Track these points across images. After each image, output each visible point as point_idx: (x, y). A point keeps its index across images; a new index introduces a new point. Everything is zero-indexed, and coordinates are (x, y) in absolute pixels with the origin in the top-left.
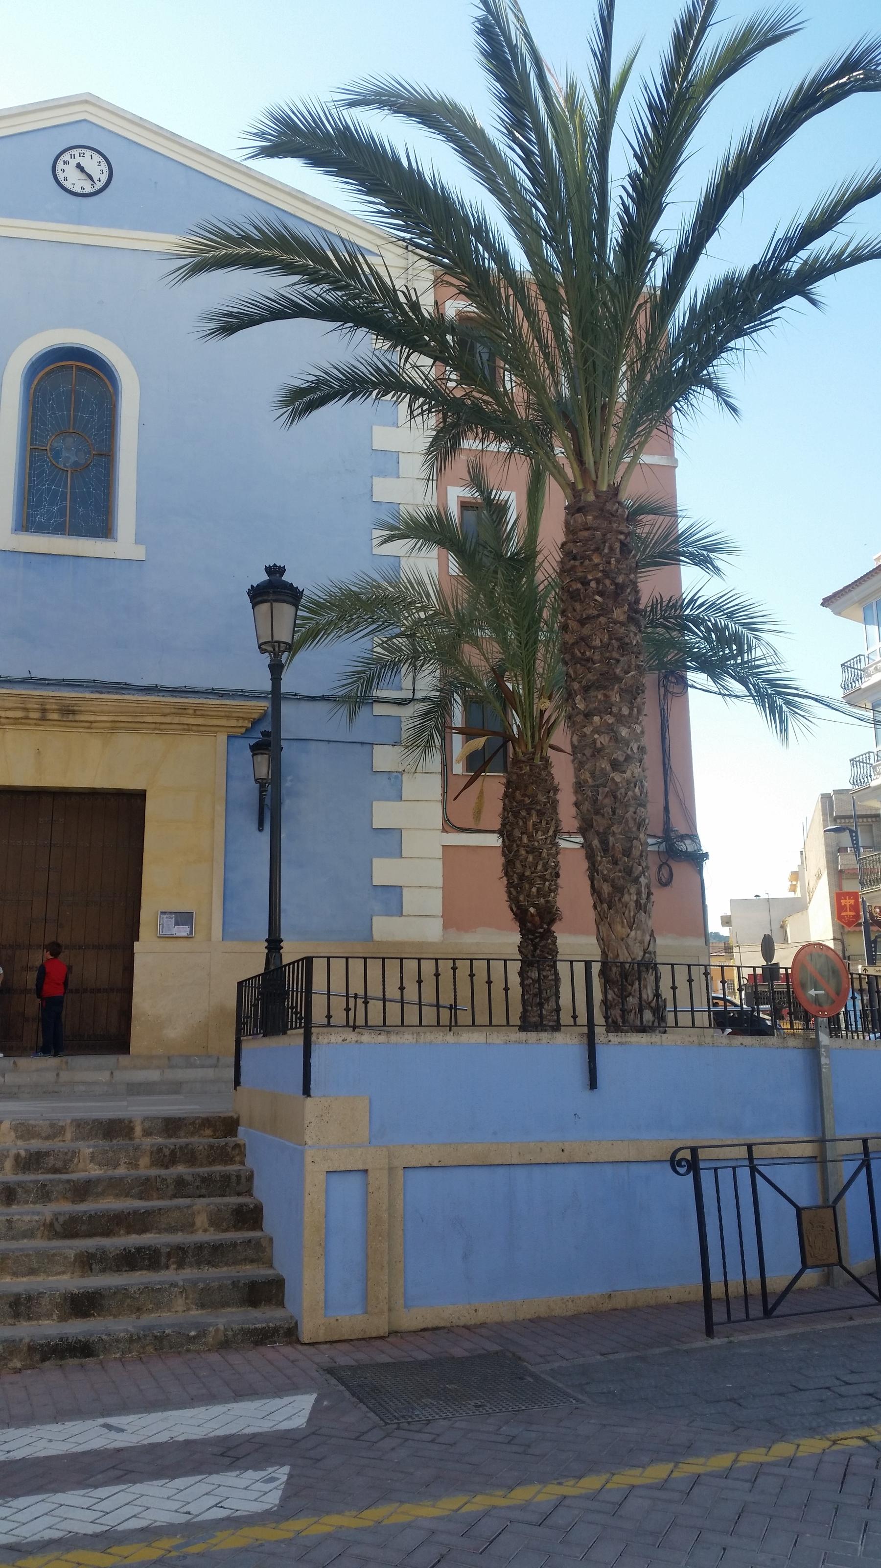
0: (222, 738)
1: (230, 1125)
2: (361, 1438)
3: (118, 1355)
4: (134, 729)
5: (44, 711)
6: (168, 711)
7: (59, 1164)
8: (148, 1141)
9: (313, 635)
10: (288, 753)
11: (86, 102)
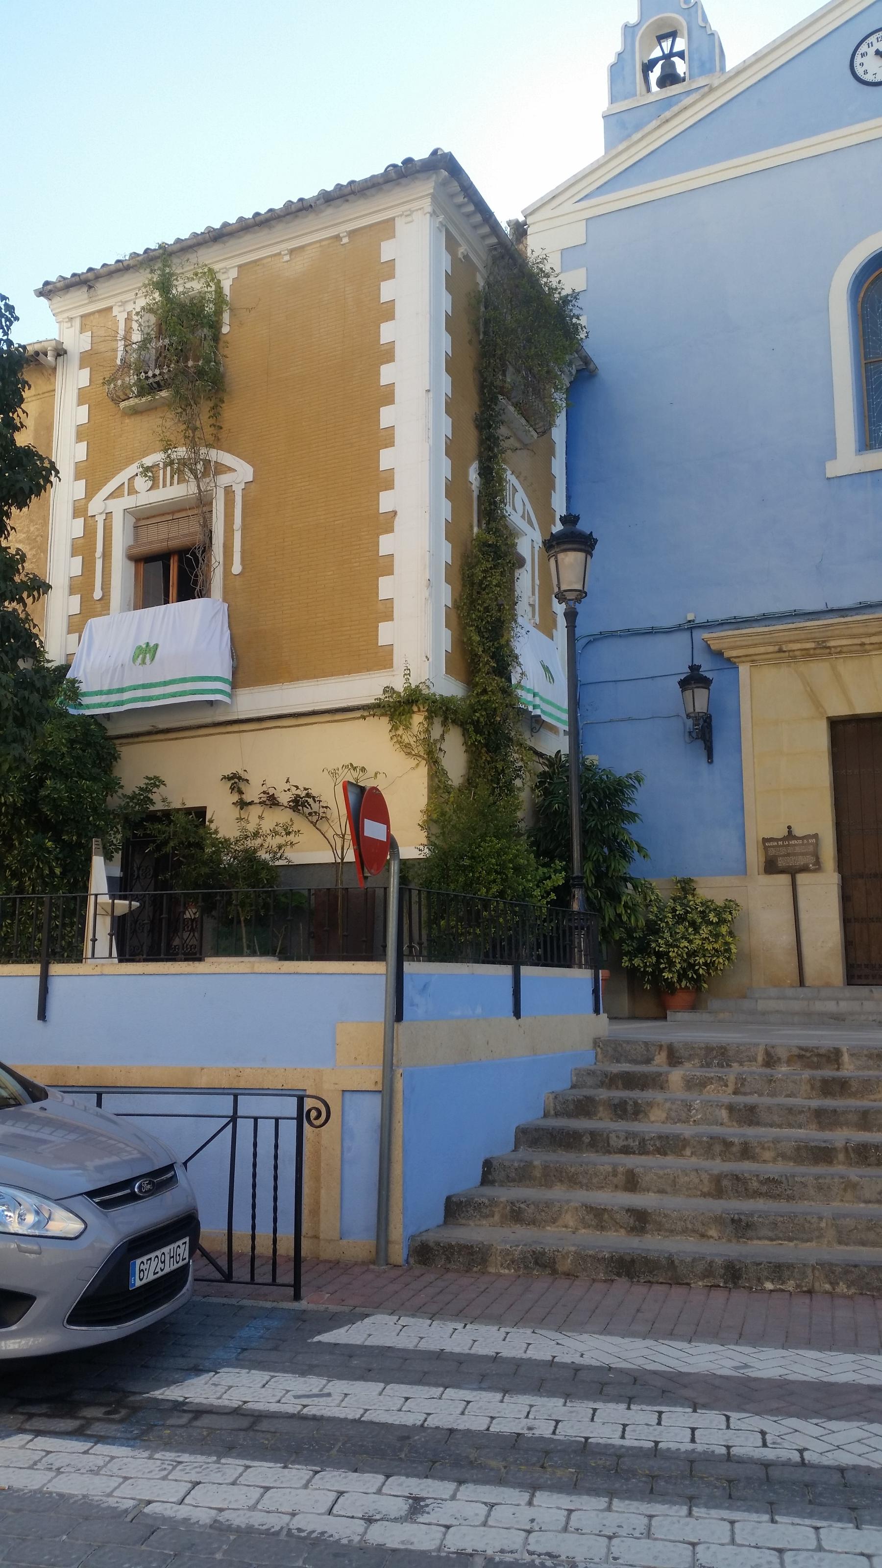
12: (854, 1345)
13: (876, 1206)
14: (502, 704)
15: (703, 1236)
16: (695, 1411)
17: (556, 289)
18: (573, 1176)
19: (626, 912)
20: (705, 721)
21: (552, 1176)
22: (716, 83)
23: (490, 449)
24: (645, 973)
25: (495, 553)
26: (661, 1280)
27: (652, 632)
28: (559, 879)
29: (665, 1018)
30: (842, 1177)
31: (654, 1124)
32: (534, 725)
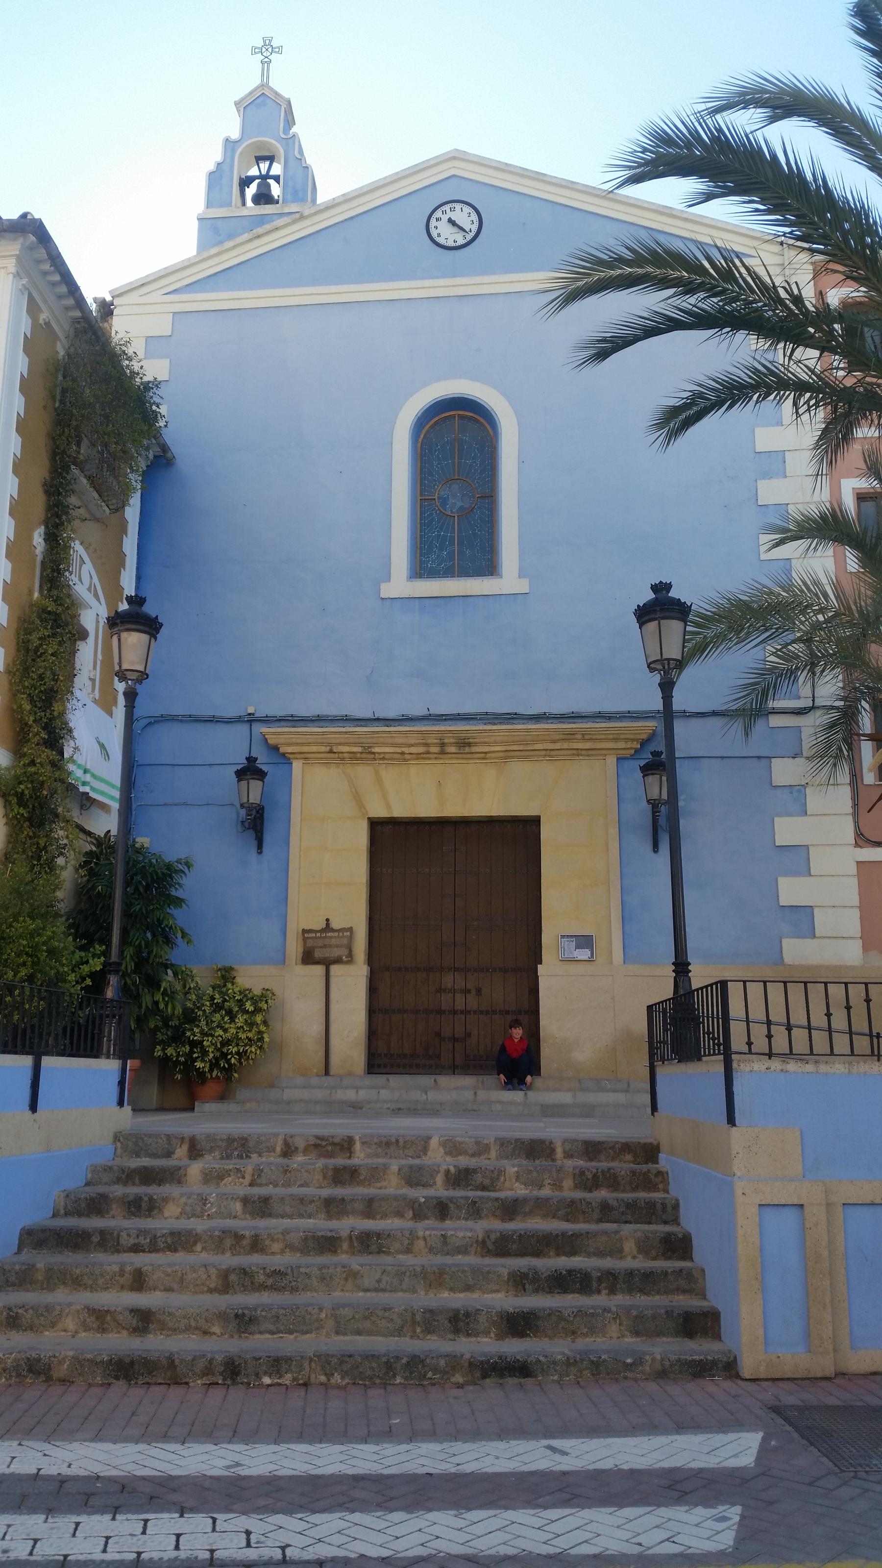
0: (612, 761)
1: (650, 1152)
2: (817, 1484)
3: (556, 1378)
4: (526, 757)
5: (443, 745)
6: (557, 737)
7: (487, 1182)
8: (570, 1164)
9: (700, 649)
10: (682, 770)
11: (454, 158)
12: (343, 1436)
13: (374, 1294)
14: (50, 777)
15: (205, 1333)
16: (182, 1516)
17: (138, 374)
18: (77, 1278)
19: (163, 999)
20: (258, 812)
21: (56, 1278)
22: (306, 213)
23: (58, 516)
24: (178, 1062)
25: (55, 621)
26: (159, 1381)
27: (213, 720)
28: (97, 965)
29: (192, 1109)
30: (344, 1267)
31: (169, 1219)
32: (85, 802)
